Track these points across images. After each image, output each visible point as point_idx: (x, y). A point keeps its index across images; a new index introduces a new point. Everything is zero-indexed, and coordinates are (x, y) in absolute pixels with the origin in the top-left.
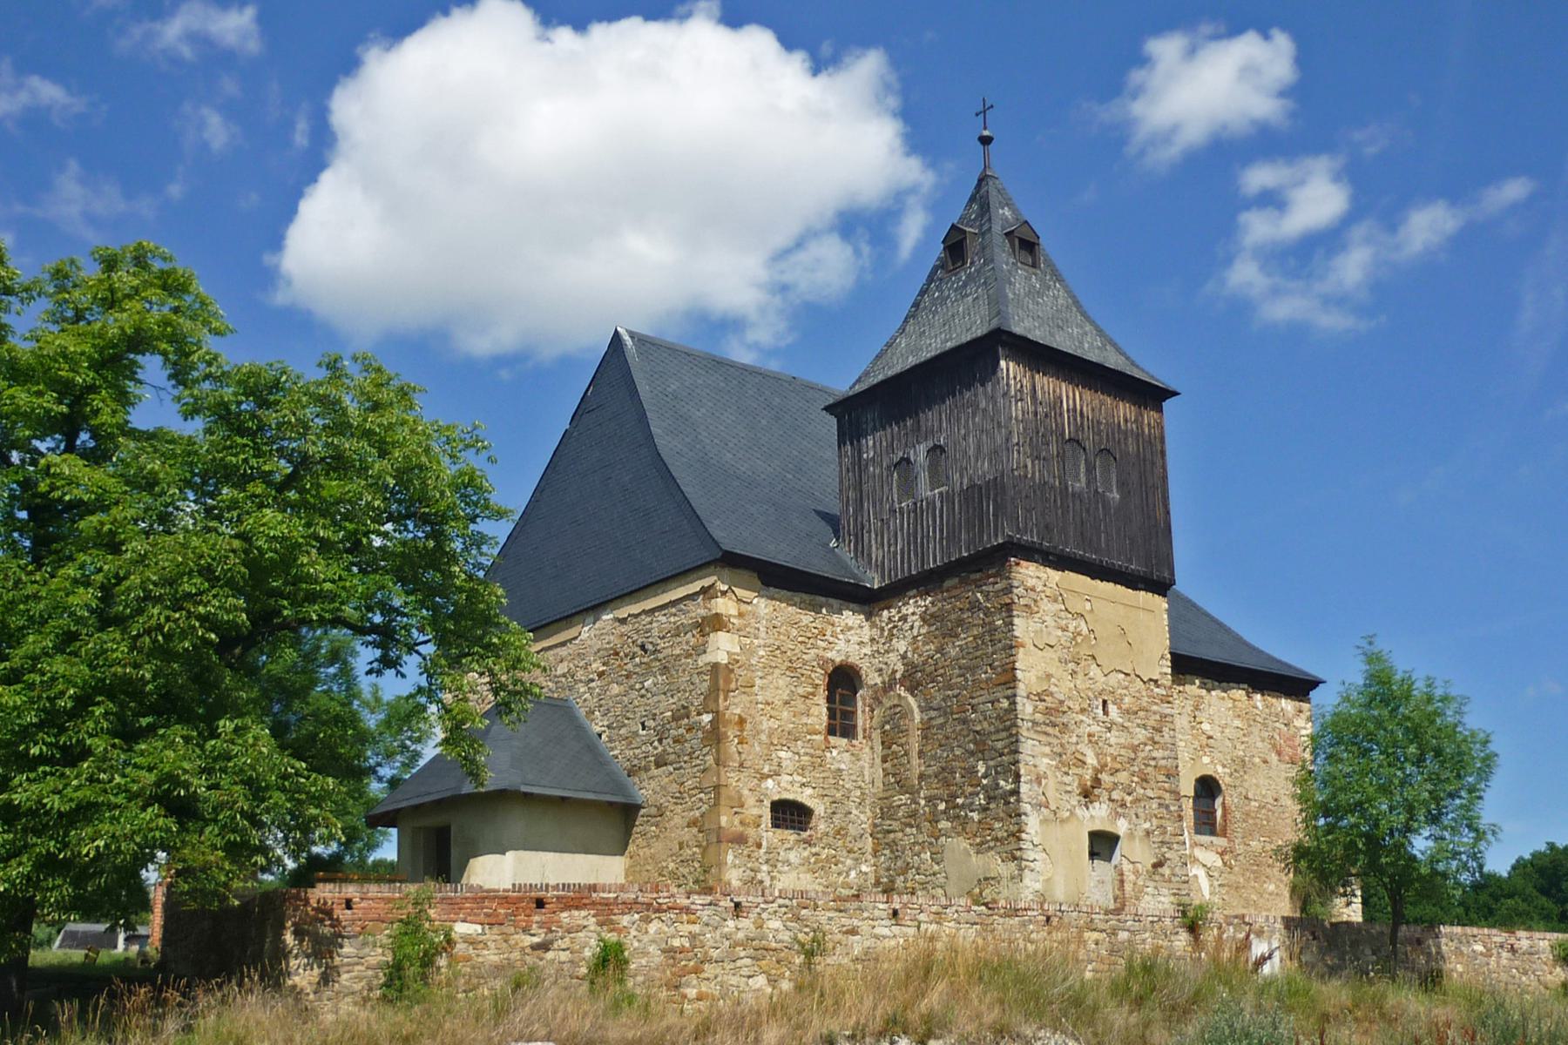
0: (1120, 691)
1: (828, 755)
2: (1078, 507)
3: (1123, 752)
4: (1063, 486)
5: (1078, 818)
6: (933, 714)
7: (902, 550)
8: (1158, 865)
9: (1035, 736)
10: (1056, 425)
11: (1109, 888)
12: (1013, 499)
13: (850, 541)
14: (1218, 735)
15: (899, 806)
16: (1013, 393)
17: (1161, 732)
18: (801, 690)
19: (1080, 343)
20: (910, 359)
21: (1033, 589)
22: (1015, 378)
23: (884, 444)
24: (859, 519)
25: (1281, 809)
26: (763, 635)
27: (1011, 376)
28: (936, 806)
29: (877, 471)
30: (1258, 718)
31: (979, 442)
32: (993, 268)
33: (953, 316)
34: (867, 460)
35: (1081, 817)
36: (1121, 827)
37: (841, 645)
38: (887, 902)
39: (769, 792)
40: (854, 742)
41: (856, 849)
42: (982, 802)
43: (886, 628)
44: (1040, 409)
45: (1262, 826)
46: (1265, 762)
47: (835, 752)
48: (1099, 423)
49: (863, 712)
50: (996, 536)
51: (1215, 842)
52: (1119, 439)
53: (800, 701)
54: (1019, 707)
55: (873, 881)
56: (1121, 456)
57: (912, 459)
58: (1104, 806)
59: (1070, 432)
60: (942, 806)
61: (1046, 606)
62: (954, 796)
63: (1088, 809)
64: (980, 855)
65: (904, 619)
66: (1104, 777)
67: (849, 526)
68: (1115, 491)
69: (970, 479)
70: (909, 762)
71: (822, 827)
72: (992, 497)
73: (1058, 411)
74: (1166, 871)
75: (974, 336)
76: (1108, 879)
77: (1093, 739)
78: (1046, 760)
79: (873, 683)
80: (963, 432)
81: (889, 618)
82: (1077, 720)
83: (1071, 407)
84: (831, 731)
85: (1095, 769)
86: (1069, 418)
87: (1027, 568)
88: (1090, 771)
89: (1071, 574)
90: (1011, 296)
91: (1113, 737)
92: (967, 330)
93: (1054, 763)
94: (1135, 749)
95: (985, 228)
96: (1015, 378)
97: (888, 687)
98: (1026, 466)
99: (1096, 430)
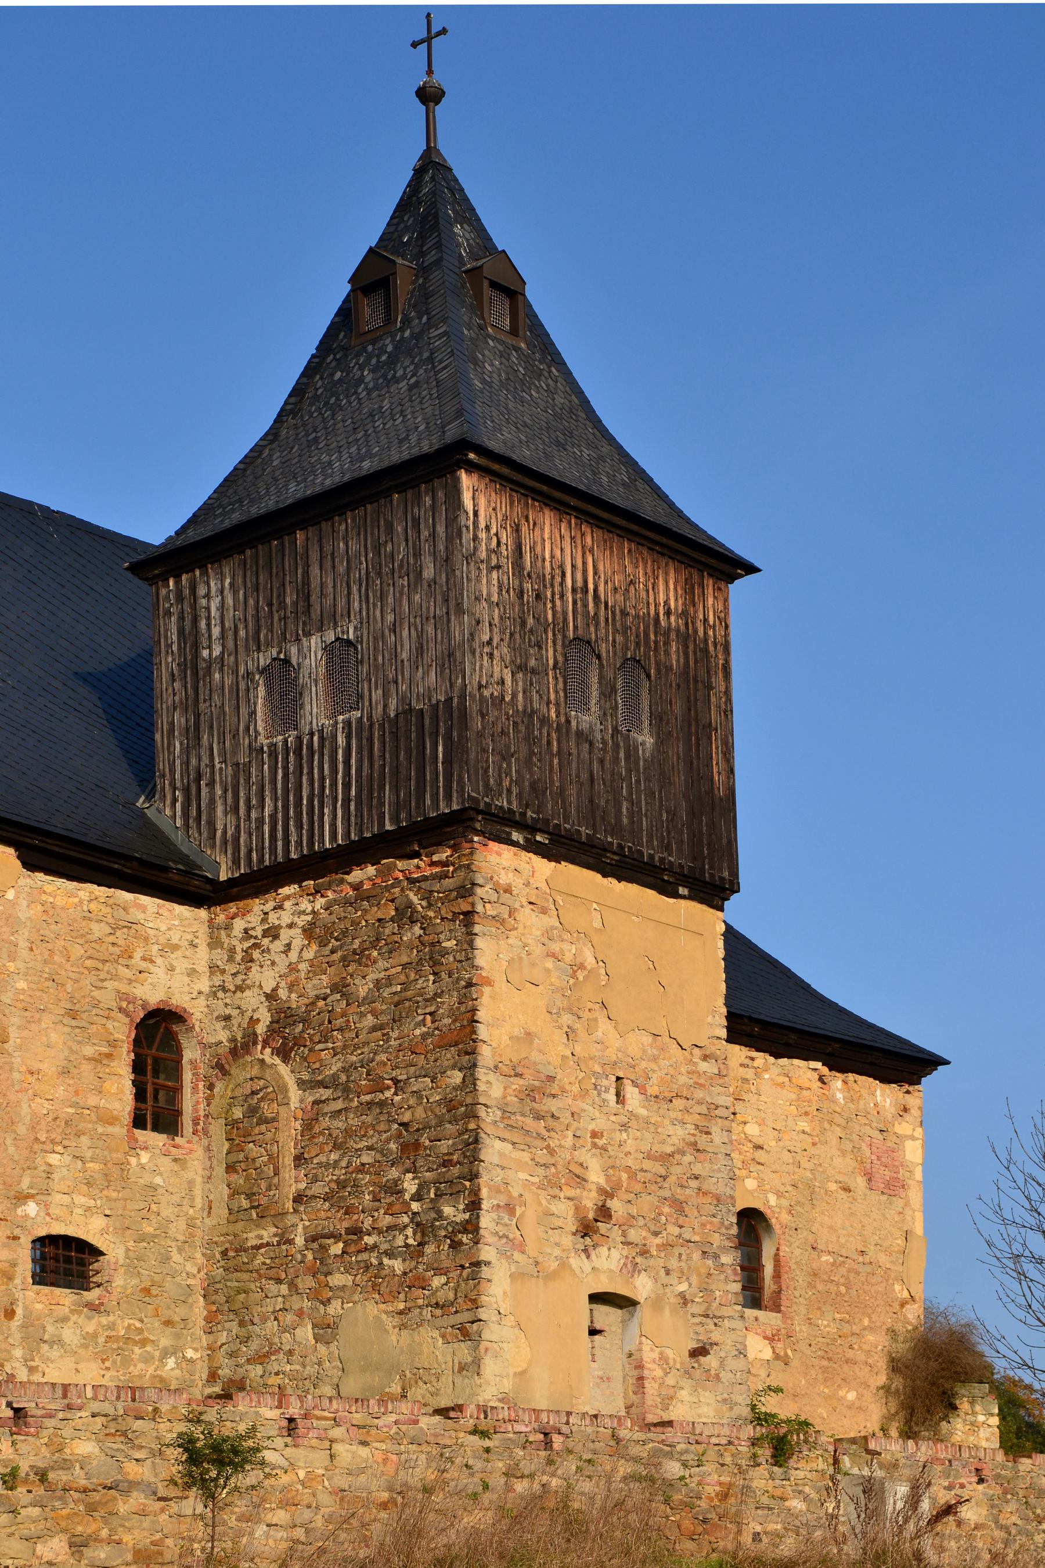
0: (644, 1064)
1: (133, 1161)
2: (585, 755)
3: (647, 1165)
4: (563, 719)
5: (574, 1274)
6: (325, 1093)
7: (273, 817)
8: (699, 1352)
9: (506, 1135)
10: (554, 615)
11: (618, 1387)
12: (480, 735)
13: (174, 800)
14: (771, 1143)
15: (258, 1247)
16: (483, 555)
17: (708, 1133)
18: (89, 1051)
19: (594, 473)
20: (292, 487)
21: (508, 890)
22: (488, 528)
23: (242, 633)
24: (194, 762)
25: (868, 1268)
26: (24, 953)
27: (482, 525)
28: (324, 1248)
29: (228, 682)
30: (838, 1119)
31: (420, 637)
32: (445, 333)
33: (371, 415)
34: (210, 662)
35: (578, 1271)
36: (642, 1288)
37: (159, 972)
38: (279, 1407)
39: (29, 1223)
40: (178, 1140)
41: (177, 1319)
42: (411, 1241)
43: (238, 949)
44: (527, 586)
45: (838, 1294)
46: (847, 1190)
47: (145, 1157)
48: (624, 613)
49: (195, 1089)
50: (448, 797)
51: (761, 1319)
52: (656, 642)
53: (87, 1067)
54: (481, 1086)
55: (205, 1376)
56: (658, 671)
57: (294, 661)
58: (615, 1254)
59: (575, 627)
60: (337, 1248)
61: (527, 916)
62: (356, 1231)
63: (588, 1257)
64: (404, 1332)
65: (272, 933)
66: (615, 1205)
67: (173, 772)
68: (646, 731)
69: (403, 699)
70: (276, 1174)
71: (119, 1281)
72: (442, 731)
73: (557, 589)
74: (710, 1361)
75: (415, 452)
76: (617, 1374)
77: (600, 1142)
78: (523, 1175)
79: (212, 1040)
80: (390, 618)
81: (246, 931)
82: (574, 1109)
83: (580, 583)
84: (139, 1122)
85: (602, 1191)
86: (575, 602)
87: (499, 854)
88: (594, 1194)
89: (571, 866)
90: (478, 384)
91: (630, 1140)
92: (401, 441)
93: (536, 1180)
94: (666, 1158)
95: (431, 258)
96: (488, 528)
97: (241, 1048)
98: (502, 682)
99: (618, 624)
